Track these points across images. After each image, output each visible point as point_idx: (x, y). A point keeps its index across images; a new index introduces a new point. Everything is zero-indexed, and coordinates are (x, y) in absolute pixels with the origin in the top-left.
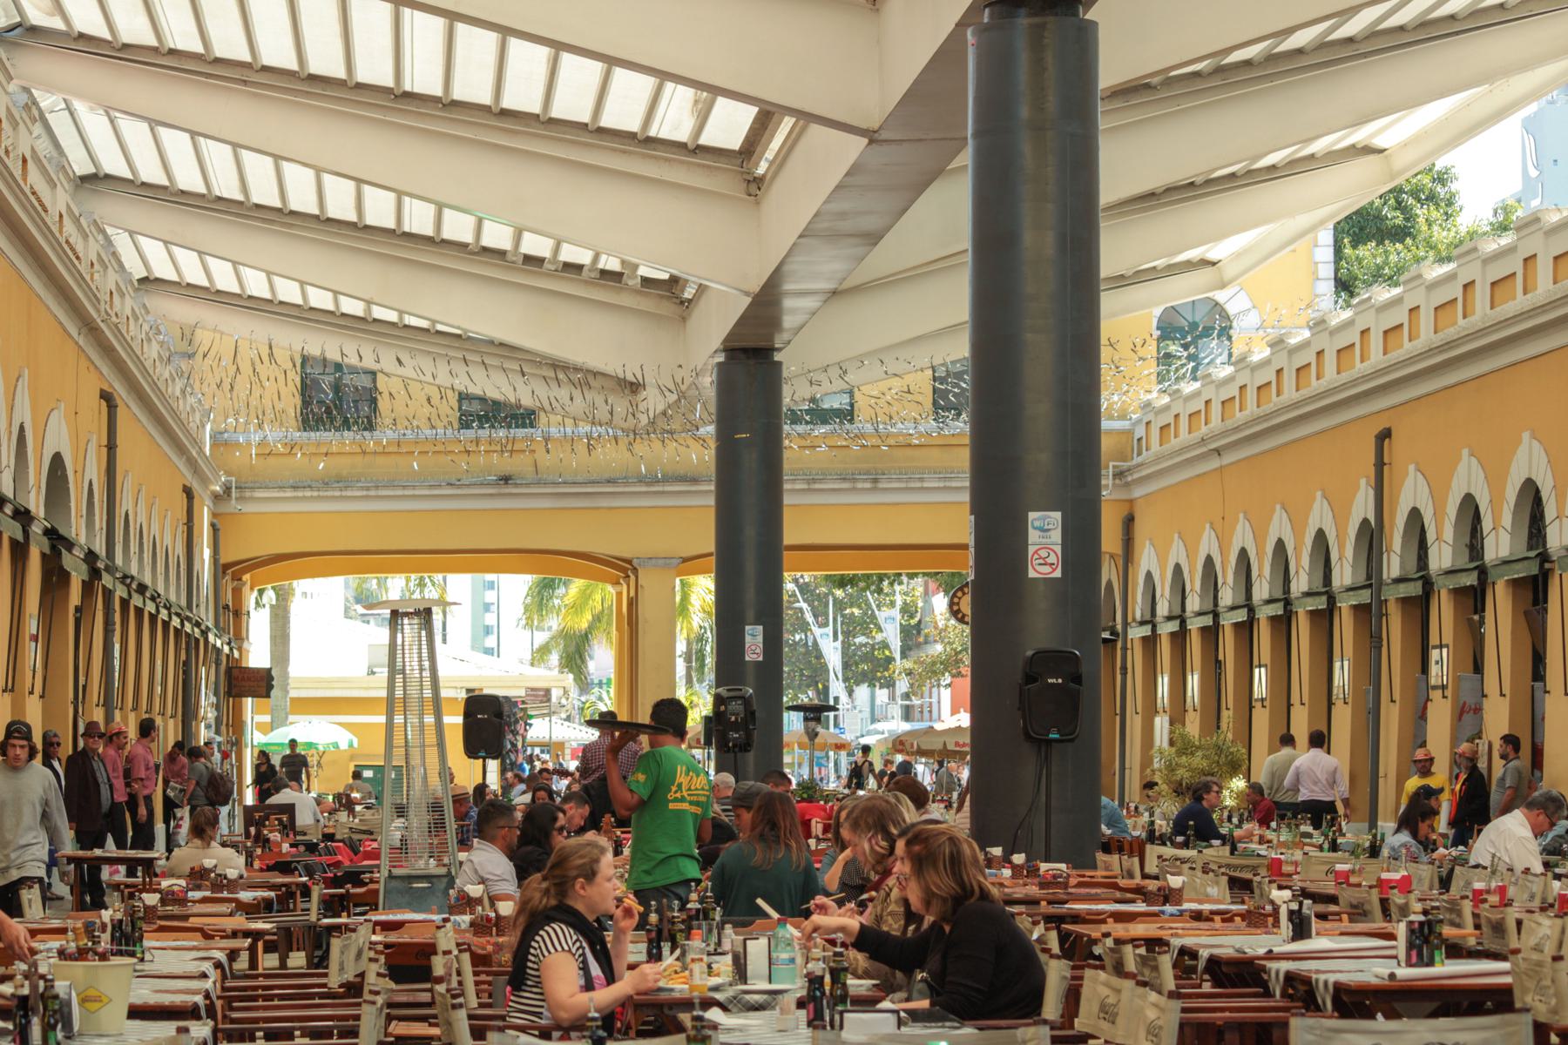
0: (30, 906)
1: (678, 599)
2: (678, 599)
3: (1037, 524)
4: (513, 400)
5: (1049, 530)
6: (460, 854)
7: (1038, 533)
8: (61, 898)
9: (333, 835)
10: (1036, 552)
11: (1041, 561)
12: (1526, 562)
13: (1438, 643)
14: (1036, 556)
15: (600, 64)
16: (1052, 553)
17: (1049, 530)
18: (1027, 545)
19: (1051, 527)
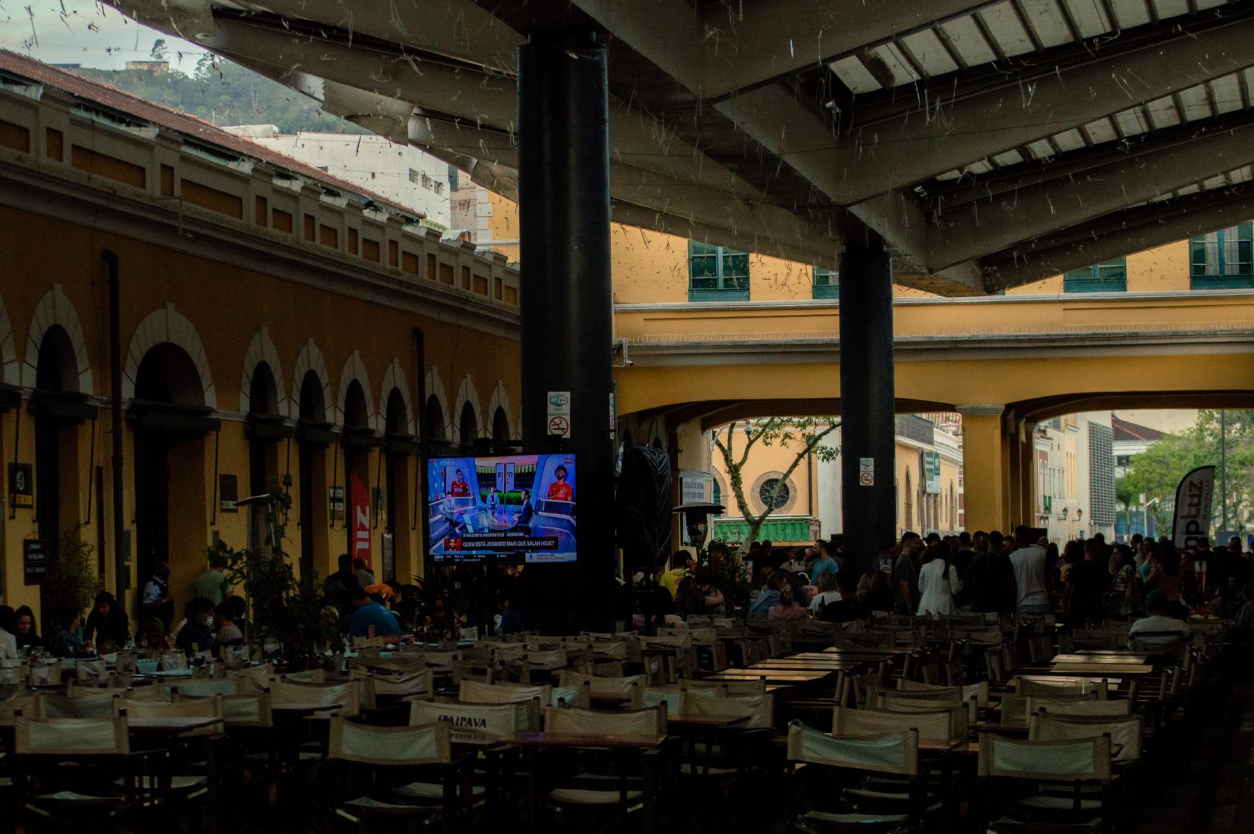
0: (981, 641)
1: (74, 764)
2: (74, 764)
3: (553, 400)
4: (450, 235)
5: (561, 405)
6: (1014, 685)
7: (553, 407)
8: (823, 597)
9: (291, 485)
10: (552, 420)
11: (556, 427)
12: (1201, 471)
13: (333, 484)
14: (552, 423)
15: (406, 103)
16: (563, 421)
17: (561, 405)
18: (547, 415)
19: (563, 402)
